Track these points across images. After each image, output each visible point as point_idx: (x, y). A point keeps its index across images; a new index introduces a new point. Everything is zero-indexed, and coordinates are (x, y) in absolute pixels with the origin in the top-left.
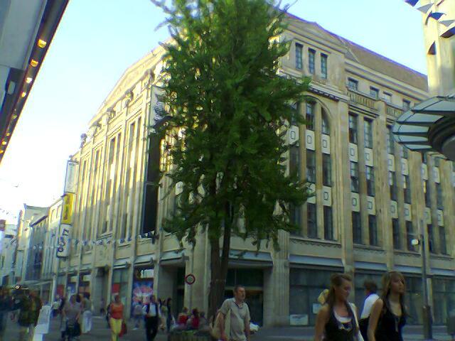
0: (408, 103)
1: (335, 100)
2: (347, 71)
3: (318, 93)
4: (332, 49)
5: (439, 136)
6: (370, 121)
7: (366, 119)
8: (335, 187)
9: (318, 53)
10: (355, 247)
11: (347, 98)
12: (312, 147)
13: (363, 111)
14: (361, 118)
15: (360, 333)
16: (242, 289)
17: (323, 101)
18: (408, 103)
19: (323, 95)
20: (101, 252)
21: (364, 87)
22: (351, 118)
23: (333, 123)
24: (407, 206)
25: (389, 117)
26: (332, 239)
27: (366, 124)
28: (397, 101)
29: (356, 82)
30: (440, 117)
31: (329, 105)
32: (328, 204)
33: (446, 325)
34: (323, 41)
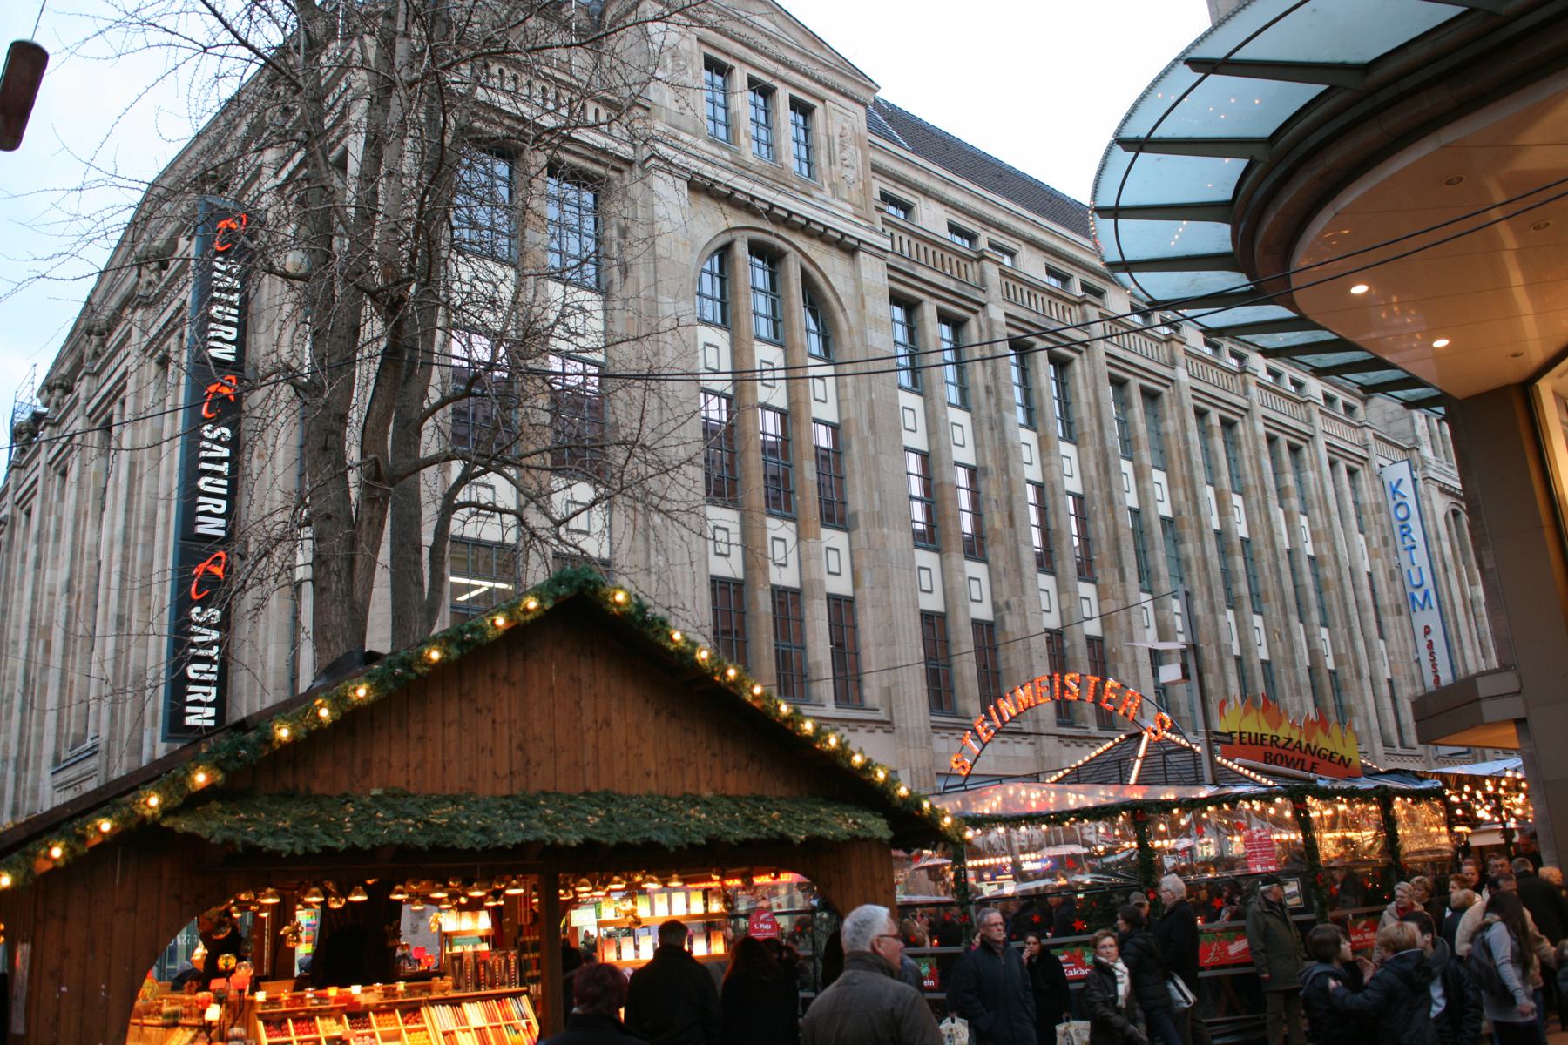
0: (1065, 279)
1: (848, 248)
2: (877, 169)
3: (787, 221)
4: (826, 85)
5: (1270, 218)
6: (957, 324)
7: (944, 317)
8: (861, 532)
9: (783, 94)
10: (936, 728)
11: (885, 244)
12: (787, 577)
13: (935, 291)
14: (929, 310)
15: (353, 499)
16: (1237, 839)
17: (805, 249)
18: (1065, 279)
19: (806, 228)
20: (219, 811)
21: (932, 218)
22: (898, 313)
23: (846, 320)
24: (1087, 589)
25: (1013, 310)
26: (860, 705)
27: (946, 331)
28: (1032, 265)
29: (907, 208)
30: (1316, 89)
31: (830, 264)
32: (842, 586)
33: (970, 903)
34: (791, 57)
